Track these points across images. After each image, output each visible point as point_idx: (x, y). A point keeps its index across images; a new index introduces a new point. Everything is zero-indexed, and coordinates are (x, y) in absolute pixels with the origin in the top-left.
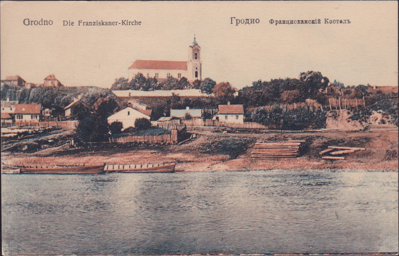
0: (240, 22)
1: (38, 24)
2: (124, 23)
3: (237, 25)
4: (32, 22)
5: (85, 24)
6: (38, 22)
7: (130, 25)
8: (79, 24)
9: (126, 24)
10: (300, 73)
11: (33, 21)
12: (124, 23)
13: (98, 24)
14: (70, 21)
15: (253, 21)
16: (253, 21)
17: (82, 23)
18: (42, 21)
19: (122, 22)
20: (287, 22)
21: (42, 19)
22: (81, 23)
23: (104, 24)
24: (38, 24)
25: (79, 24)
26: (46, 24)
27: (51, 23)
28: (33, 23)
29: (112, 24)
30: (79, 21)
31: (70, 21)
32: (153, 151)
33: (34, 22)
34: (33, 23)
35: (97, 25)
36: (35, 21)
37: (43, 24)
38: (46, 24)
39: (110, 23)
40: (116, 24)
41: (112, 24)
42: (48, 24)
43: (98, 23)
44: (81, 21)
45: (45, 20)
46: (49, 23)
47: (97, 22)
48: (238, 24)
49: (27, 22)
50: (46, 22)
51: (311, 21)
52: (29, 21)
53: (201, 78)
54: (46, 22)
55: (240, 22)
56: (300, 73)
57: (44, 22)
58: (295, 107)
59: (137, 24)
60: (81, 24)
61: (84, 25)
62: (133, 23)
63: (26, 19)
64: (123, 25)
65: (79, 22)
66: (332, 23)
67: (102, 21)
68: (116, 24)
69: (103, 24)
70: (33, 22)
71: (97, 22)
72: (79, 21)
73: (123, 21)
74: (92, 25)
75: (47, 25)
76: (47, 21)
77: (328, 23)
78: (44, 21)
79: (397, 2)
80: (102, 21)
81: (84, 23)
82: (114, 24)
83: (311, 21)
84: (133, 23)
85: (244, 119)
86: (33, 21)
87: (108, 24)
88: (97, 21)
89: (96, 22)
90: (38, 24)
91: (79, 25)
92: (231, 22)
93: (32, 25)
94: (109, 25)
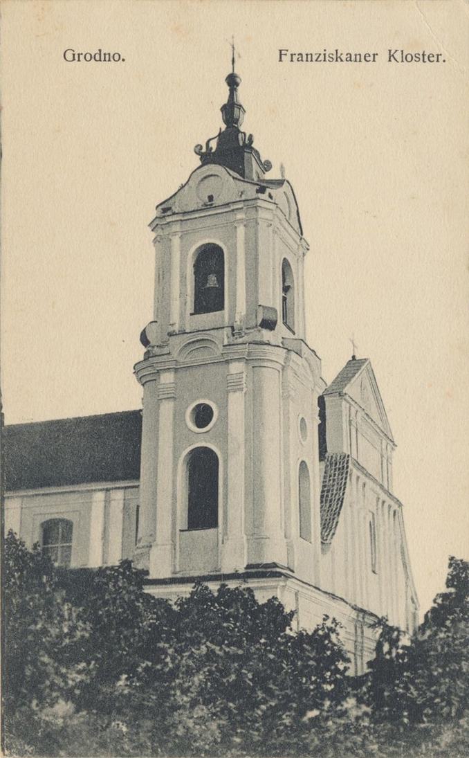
0: (93, 56)
1: (93, 59)
2: (394, 58)
4: (79, 55)
5: (295, 58)
7: (79, 60)
8: (281, 57)
9: (399, 59)
10: (453, 562)
12: (393, 55)
13: (327, 58)
15: (424, 57)
16: (424, 57)
17: (289, 57)
20: (307, 58)
21: (100, 50)
22: (286, 55)
23: (344, 57)
24: (93, 59)
25: (281, 57)
26: (107, 59)
27: (117, 57)
28: (82, 57)
29: (363, 57)
35: (325, 60)
36: (85, 55)
40: (438, 59)
41: (363, 57)
42: (112, 59)
43: (327, 56)
44: (287, 50)
47: (325, 55)
50: (107, 56)
51: (370, 56)
52: (74, 55)
55: (93, 56)
56: (453, 562)
58: (77, 632)
59: (109, 60)
60: (286, 59)
61: (292, 61)
65: (281, 55)
67: (337, 51)
68: (438, 59)
69: (338, 59)
71: (325, 55)
72: (281, 51)
74: (312, 61)
75: (360, 61)
77: (342, 60)
78: (105, 54)
79: (9, 421)
80: (337, 51)
81: (292, 55)
82: (432, 59)
83: (333, 54)
85: (448, 578)
87: (304, 58)
88: (325, 50)
90: (114, 55)
93: (79, 60)
94: (105, 60)
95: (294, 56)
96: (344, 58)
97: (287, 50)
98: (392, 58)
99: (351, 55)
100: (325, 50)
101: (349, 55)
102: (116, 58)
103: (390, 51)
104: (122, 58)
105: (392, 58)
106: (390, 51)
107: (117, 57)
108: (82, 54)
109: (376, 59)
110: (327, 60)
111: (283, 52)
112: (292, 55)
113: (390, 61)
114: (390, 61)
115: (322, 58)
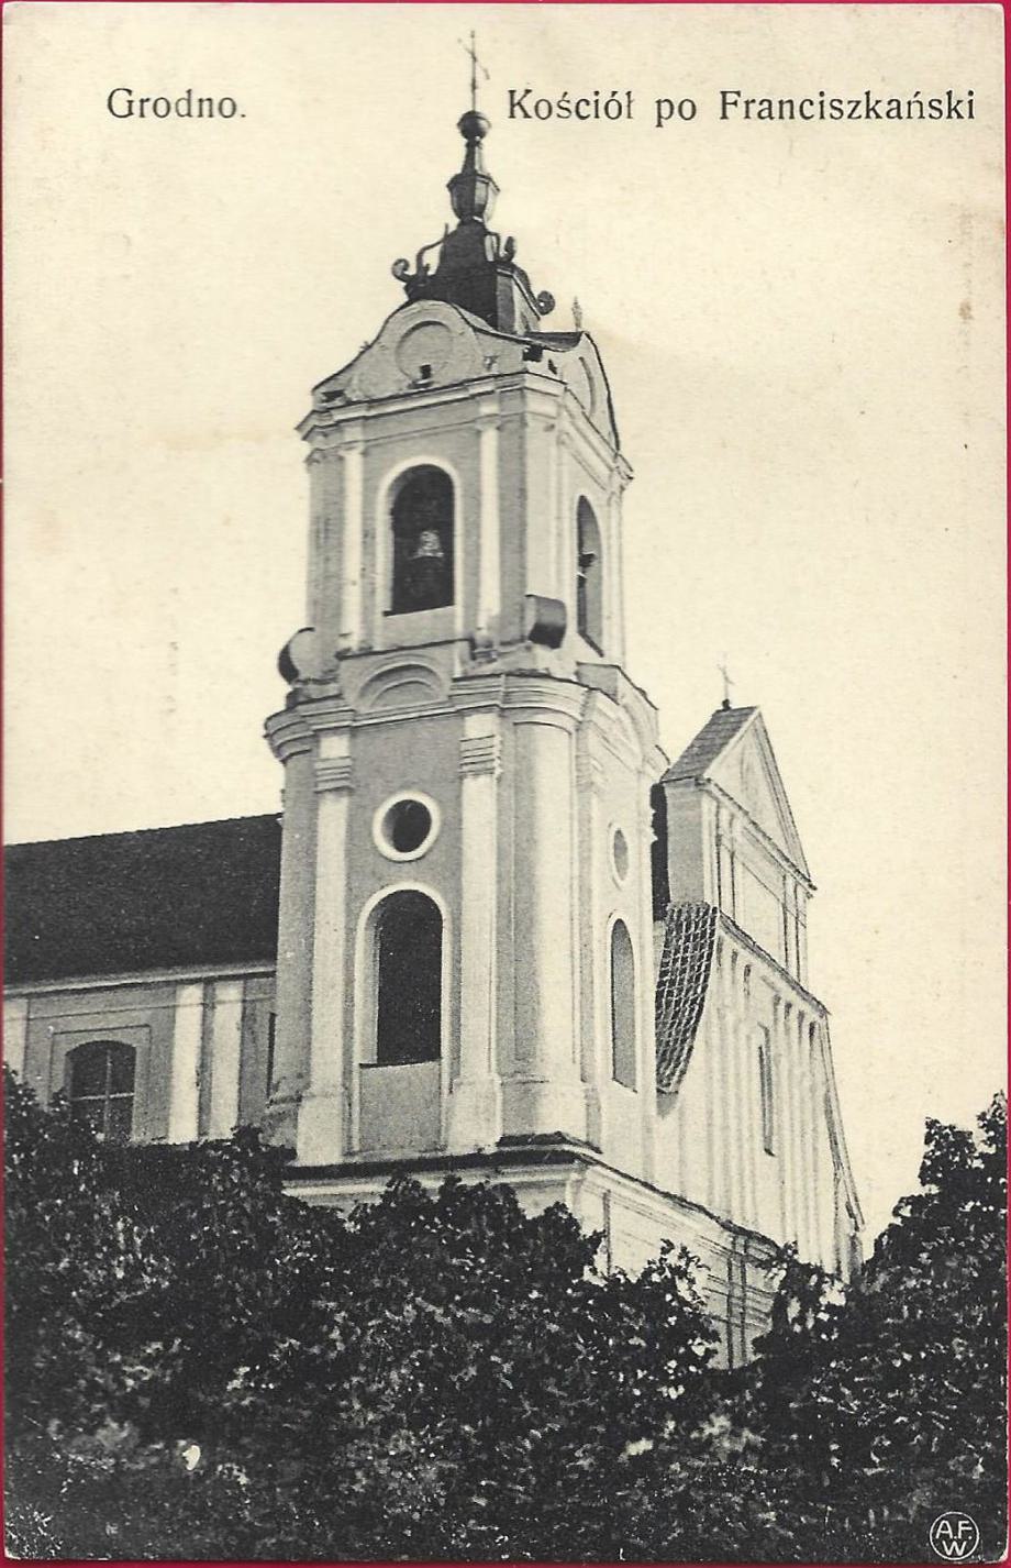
2: (957, 112)
3: (659, 125)
5: (754, 109)
6: (177, 111)
11: (148, 100)
13: (828, 110)
14: (597, 93)
17: (741, 105)
18: (189, 101)
19: (512, 98)
22: (735, 103)
23: (882, 109)
26: (206, 112)
27: (687, 111)
28: (148, 106)
30: (724, 93)
31: (822, 94)
32: (494, 969)
33: (151, 103)
34: (148, 106)
36: (156, 101)
37: (195, 111)
38: (206, 112)
39: (787, 107)
43: (827, 104)
44: (738, 93)
45: (205, 98)
46: (607, 113)
48: (186, 96)
49: (120, 106)
51: (588, 103)
53: (185, 1006)
54: (206, 105)
57: (784, 115)
62: (583, 104)
63: (114, 92)
64: (868, 116)
65: (724, 103)
66: (173, 113)
67: (949, 93)
70: (145, 104)
72: (724, 93)
73: (517, 98)
75: (211, 116)
76: (791, 102)
77: (878, 116)
80: (949, 93)
81: (747, 103)
83: (588, 103)
84: (583, 104)
86: (148, 100)
88: (822, 94)
89: (592, 99)
91: (724, 117)
92: (656, 124)
93: (142, 115)
95: (751, 105)
96: (883, 114)
97: (738, 93)
98: (517, 108)
99: (770, 102)
100: (597, 93)
101: (894, 104)
102: (227, 108)
103: (512, 92)
104: (240, 111)
105: (517, 108)
106: (512, 92)
107: (687, 111)
108: (753, 101)
109: (728, 114)
110: (826, 115)
111: (731, 98)
112: (747, 103)
113: (512, 116)
114: (512, 116)
115: (861, 110)
